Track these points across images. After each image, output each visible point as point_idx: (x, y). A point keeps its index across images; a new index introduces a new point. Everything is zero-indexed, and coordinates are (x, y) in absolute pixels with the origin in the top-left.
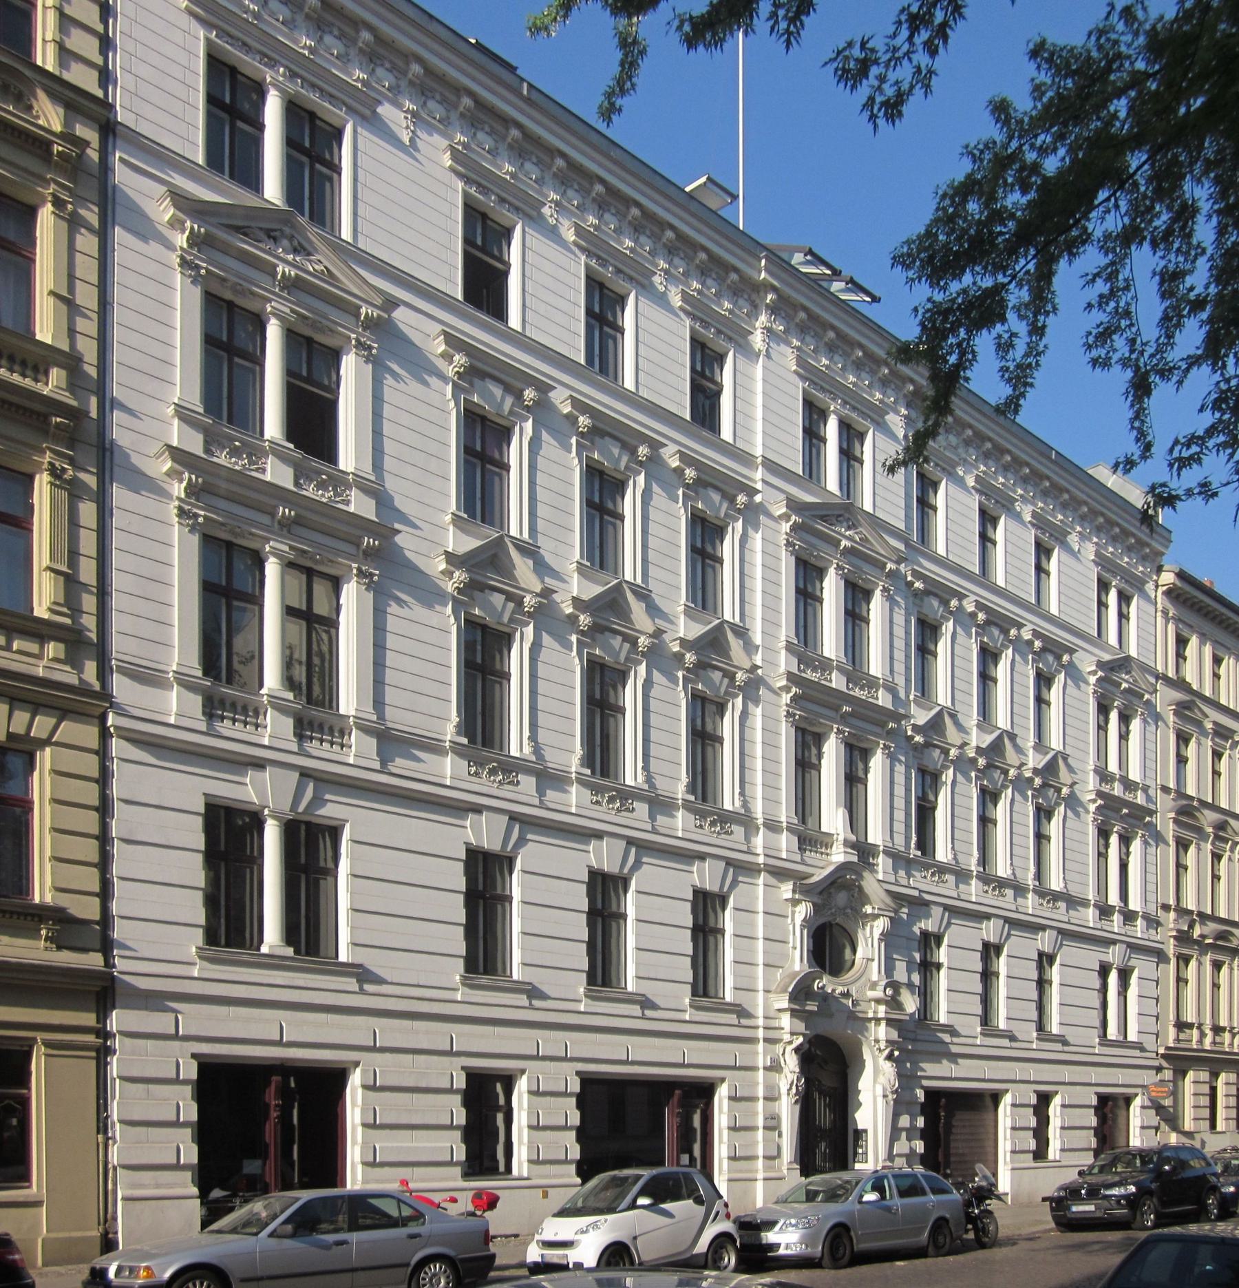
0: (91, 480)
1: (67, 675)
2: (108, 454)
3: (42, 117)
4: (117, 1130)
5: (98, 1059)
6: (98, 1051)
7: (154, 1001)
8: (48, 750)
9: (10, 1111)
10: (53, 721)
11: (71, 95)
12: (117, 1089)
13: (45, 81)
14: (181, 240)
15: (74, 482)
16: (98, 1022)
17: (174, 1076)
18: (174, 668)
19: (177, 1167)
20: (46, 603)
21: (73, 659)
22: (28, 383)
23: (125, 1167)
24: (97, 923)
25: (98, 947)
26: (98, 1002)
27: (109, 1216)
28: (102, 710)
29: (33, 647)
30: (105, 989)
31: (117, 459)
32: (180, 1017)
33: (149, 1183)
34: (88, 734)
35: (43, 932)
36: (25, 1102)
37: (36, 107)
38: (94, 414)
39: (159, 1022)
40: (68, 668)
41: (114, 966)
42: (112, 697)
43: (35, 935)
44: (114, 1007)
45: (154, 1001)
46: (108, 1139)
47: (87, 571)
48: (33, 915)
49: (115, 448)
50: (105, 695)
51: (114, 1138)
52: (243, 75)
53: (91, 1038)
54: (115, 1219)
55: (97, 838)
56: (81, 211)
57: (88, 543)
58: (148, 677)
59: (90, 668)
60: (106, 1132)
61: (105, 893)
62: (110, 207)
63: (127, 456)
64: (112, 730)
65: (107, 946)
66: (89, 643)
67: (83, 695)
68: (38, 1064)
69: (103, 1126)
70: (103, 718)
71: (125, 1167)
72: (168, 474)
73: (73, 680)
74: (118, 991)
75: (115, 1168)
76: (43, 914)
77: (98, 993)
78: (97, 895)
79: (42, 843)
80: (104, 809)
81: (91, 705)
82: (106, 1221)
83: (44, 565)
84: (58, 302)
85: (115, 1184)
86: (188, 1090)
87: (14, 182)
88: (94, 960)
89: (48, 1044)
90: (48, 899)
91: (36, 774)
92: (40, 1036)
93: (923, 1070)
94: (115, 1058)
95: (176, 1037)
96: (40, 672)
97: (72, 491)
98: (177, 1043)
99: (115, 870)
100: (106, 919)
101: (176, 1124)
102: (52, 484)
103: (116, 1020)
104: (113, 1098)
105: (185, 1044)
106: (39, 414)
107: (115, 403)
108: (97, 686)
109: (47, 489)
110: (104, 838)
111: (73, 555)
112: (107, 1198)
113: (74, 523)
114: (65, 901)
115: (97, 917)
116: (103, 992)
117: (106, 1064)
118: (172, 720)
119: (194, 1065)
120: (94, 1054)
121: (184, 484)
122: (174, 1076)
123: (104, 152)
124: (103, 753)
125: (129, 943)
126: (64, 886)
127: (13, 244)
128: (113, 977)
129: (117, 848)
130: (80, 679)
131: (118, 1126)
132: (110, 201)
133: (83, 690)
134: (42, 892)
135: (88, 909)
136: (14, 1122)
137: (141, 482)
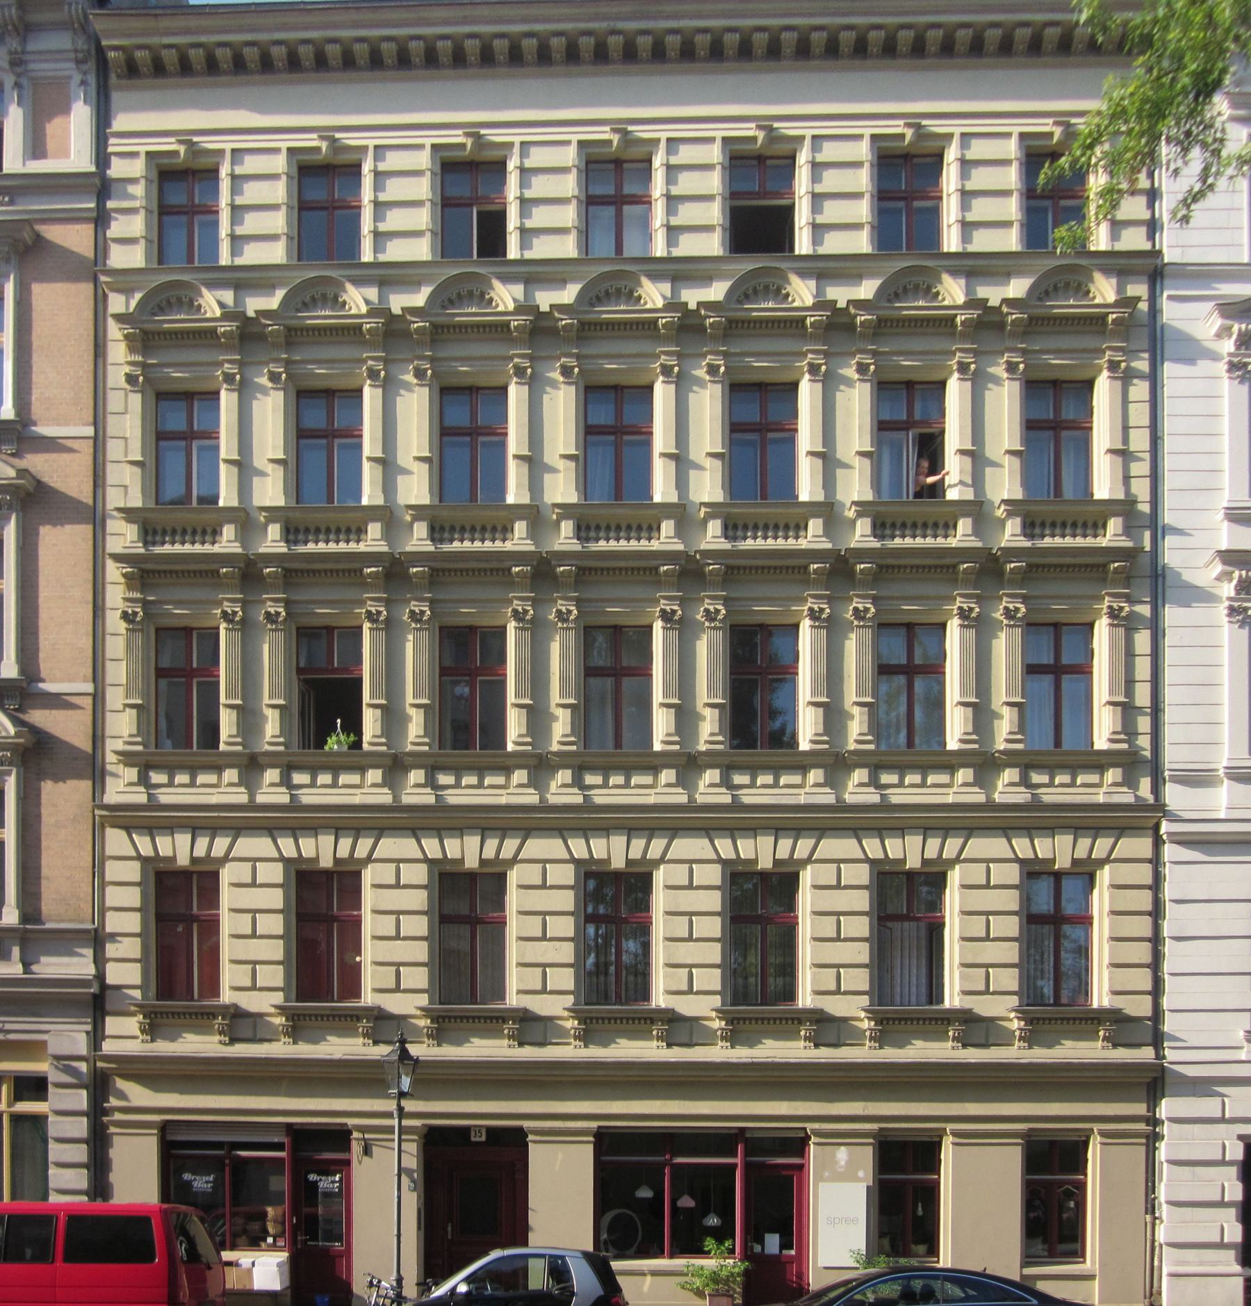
0: (1145, 610)
1: (1126, 797)
2: (1160, 579)
3: (797, 299)
4: (1164, 1211)
5: (1147, 1145)
6: (1147, 1137)
7: (1202, 1087)
8: (1107, 867)
9: (1069, 1195)
10: (1112, 840)
11: (1122, 261)
12: (1165, 1171)
13: (1096, 261)
14: (1228, 346)
15: (1132, 616)
16: (1148, 1111)
17: (1220, 1157)
18: (1225, 763)
19: (1221, 1245)
20: (809, 736)
21: (1130, 781)
22: (1089, 542)
23: (1170, 1245)
24: (1149, 1019)
25: (1150, 1040)
26: (1148, 1092)
27: (1155, 1290)
28: (1155, 821)
29: (1094, 778)
30: (1155, 1079)
31: (1169, 581)
32: (1226, 1100)
33: (1193, 1261)
34: (1140, 846)
35: (1101, 1033)
36: (1082, 1186)
37: (1093, 290)
38: (1148, 548)
39: (1207, 1106)
40: (1125, 789)
41: (1164, 1057)
42: (1165, 805)
43: (1093, 1036)
44: (1163, 1096)
45: (1202, 1087)
46: (1155, 1218)
47: (1142, 697)
48: (1092, 1019)
49: (1168, 572)
50: (1159, 807)
51: (1160, 1218)
52: (772, 158)
53: (1141, 1126)
54: (1160, 1293)
55: (1149, 940)
56: (1133, 364)
57: (1143, 668)
58: (1198, 779)
59: (1145, 785)
60: (1153, 1212)
61: (1157, 991)
62: (1159, 346)
63: (1179, 574)
64: (1165, 837)
65: (1157, 1039)
66: (1144, 761)
67: (294, 811)
68: (1094, 1153)
69: (1151, 1207)
70: (1157, 827)
71: (1170, 1245)
72: (1218, 579)
73: (1128, 798)
74: (1168, 1080)
75: (1161, 1246)
76: (950, 1017)
77: (1148, 1083)
78: (1148, 993)
79: (1101, 952)
80: (1157, 913)
81: (1145, 819)
82: (1151, 1294)
83: (1104, 701)
84: (1114, 457)
85: (1161, 1261)
86: (1233, 1171)
87: (185, 378)
88: (1146, 1054)
89: (955, 1134)
90: (1106, 1003)
91: (1096, 892)
92: (1096, 1127)
93: (122, 1096)
94: (1163, 1143)
95: (1222, 1120)
96: (1101, 799)
97: (1126, 624)
98: (1223, 1127)
99: (1167, 967)
100: (1157, 1014)
101: (1221, 1204)
102: (1110, 625)
103: (1166, 1108)
104: (1161, 1180)
105: (1231, 1126)
106: (1098, 566)
107: (1166, 530)
108: (1151, 799)
109: (660, 632)
110: (1156, 940)
111: (1130, 683)
112: (1153, 1272)
113: (1130, 654)
114: (1121, 1003)
115: (1149, 1014)
116: (1155, 1083)
117: (1155, 1149)
118: (1222, 815)
119: (1240, 1147)
120: (592, 1139)
121: (1235, 582)
122: (1220, 1157)
123: (1153, 299)
124: (1156, 861)
125: (1177, 1035)
126: (1120, 989)
127: (1074, 421)
128: (1163, 1068)
129: (1168, 947)
130: (1136, 796)
131: (1165, 1207)
132: (1159, 342)
133: (1140, 806)
134: (1100, 997)
135: (1140, 1007)
136: (1072, 1204)
137: (1196, 595)
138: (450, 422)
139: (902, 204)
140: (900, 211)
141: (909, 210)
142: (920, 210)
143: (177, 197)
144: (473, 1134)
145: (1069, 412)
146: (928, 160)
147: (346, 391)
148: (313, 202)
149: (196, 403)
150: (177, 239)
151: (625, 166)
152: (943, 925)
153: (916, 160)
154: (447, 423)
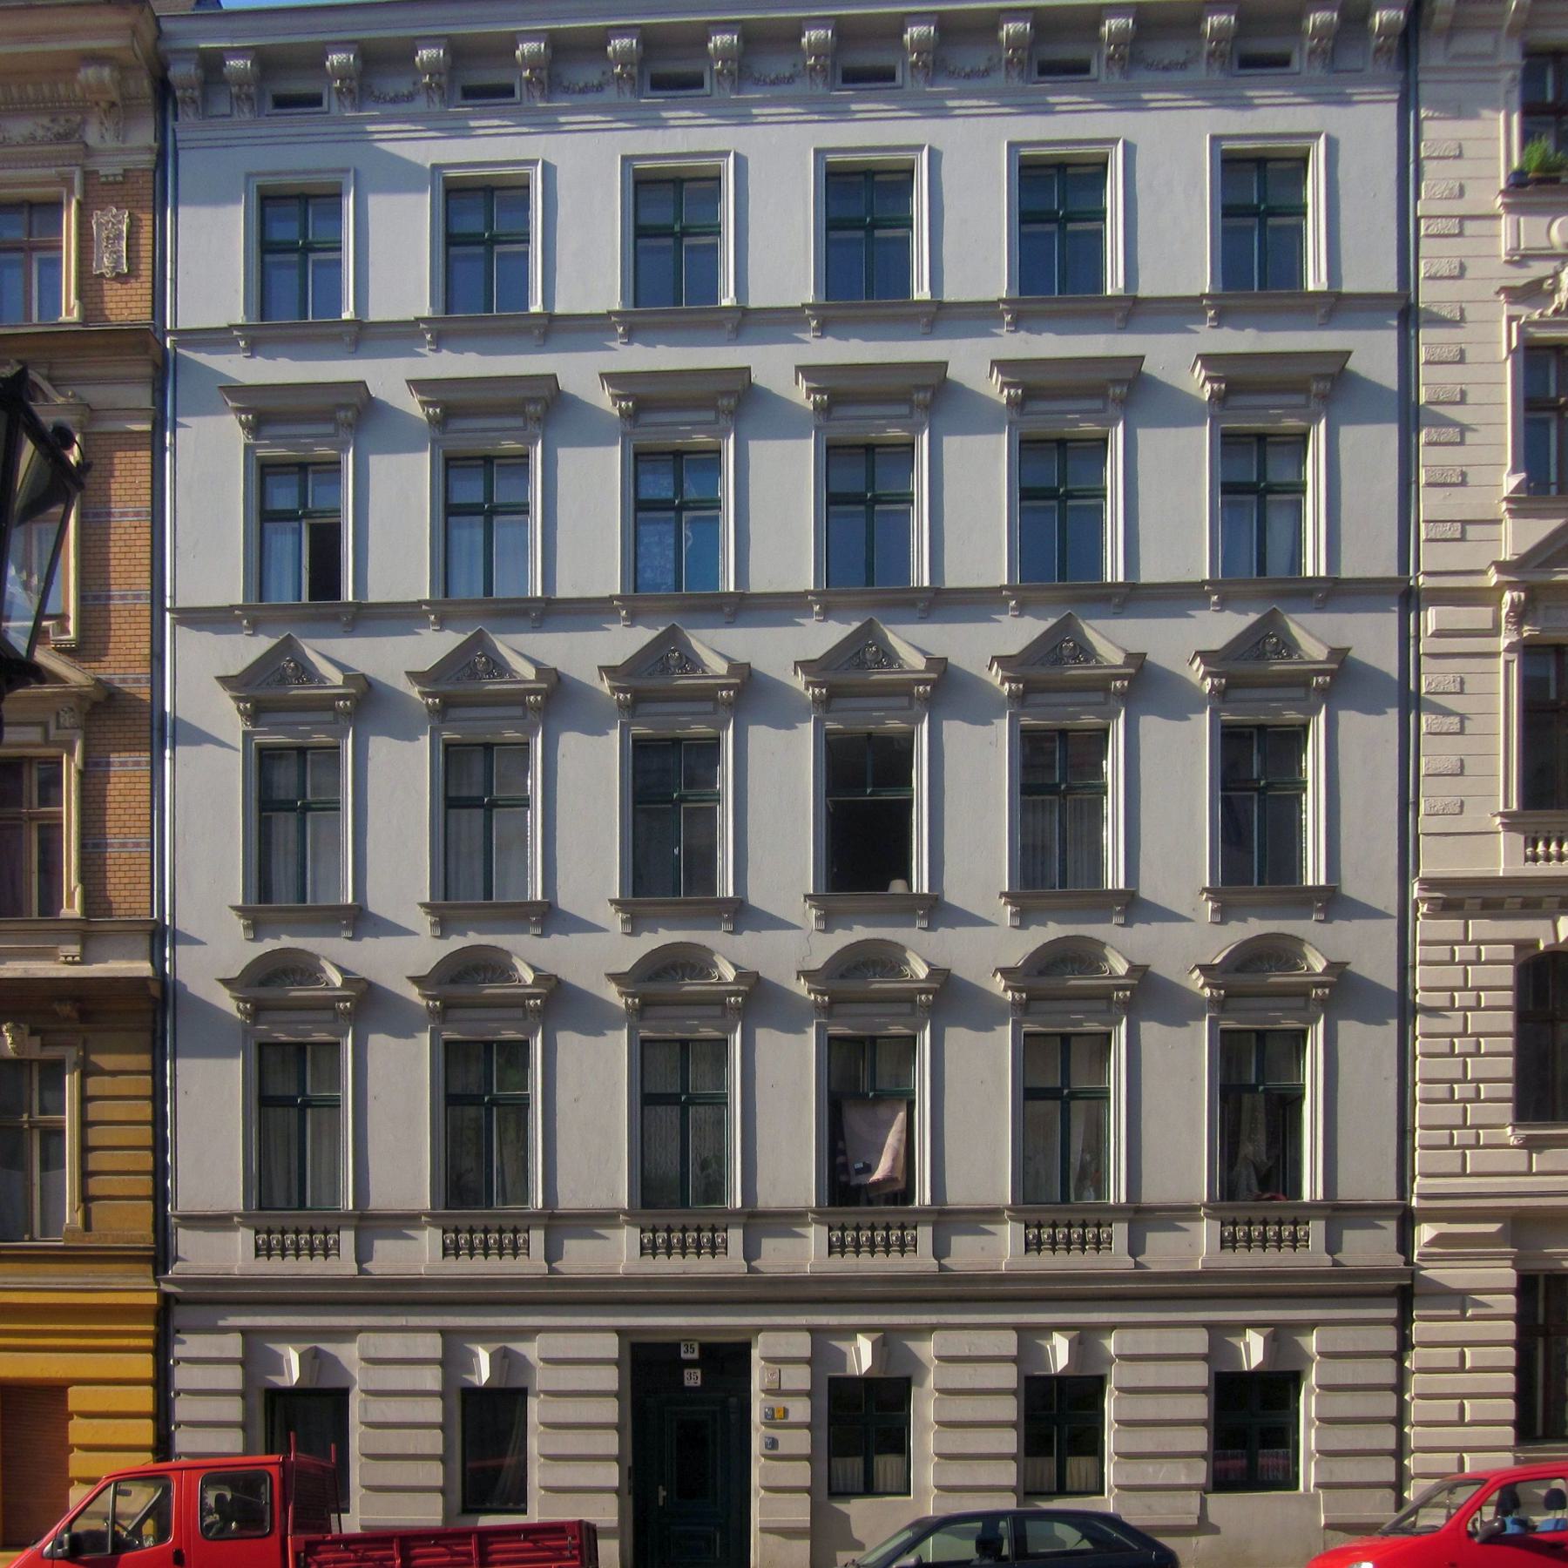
120: (151, 1327)
138: (648, 493)
139: (1053, 227)
140: (1252, 229)
141: (1263, 226)
142: (1076, 234)
143: (285, 231)
144: (683, 1349)
145: (1278, 473)
146: (1089, 170)
147: (652, 454)
148: (463, 235)
149: (310, 477)
150: (285, 281)
151: (1269, 165)
152: (1300, 1098)
153: (878, 178)
154: (643, 496)
